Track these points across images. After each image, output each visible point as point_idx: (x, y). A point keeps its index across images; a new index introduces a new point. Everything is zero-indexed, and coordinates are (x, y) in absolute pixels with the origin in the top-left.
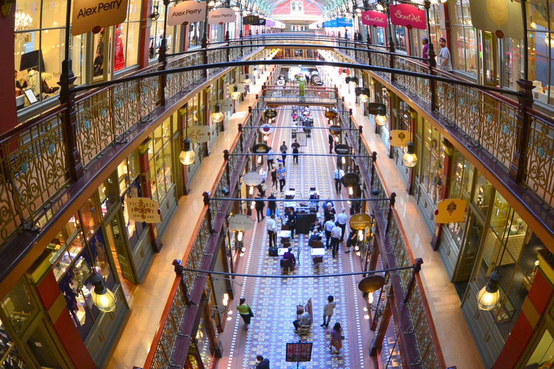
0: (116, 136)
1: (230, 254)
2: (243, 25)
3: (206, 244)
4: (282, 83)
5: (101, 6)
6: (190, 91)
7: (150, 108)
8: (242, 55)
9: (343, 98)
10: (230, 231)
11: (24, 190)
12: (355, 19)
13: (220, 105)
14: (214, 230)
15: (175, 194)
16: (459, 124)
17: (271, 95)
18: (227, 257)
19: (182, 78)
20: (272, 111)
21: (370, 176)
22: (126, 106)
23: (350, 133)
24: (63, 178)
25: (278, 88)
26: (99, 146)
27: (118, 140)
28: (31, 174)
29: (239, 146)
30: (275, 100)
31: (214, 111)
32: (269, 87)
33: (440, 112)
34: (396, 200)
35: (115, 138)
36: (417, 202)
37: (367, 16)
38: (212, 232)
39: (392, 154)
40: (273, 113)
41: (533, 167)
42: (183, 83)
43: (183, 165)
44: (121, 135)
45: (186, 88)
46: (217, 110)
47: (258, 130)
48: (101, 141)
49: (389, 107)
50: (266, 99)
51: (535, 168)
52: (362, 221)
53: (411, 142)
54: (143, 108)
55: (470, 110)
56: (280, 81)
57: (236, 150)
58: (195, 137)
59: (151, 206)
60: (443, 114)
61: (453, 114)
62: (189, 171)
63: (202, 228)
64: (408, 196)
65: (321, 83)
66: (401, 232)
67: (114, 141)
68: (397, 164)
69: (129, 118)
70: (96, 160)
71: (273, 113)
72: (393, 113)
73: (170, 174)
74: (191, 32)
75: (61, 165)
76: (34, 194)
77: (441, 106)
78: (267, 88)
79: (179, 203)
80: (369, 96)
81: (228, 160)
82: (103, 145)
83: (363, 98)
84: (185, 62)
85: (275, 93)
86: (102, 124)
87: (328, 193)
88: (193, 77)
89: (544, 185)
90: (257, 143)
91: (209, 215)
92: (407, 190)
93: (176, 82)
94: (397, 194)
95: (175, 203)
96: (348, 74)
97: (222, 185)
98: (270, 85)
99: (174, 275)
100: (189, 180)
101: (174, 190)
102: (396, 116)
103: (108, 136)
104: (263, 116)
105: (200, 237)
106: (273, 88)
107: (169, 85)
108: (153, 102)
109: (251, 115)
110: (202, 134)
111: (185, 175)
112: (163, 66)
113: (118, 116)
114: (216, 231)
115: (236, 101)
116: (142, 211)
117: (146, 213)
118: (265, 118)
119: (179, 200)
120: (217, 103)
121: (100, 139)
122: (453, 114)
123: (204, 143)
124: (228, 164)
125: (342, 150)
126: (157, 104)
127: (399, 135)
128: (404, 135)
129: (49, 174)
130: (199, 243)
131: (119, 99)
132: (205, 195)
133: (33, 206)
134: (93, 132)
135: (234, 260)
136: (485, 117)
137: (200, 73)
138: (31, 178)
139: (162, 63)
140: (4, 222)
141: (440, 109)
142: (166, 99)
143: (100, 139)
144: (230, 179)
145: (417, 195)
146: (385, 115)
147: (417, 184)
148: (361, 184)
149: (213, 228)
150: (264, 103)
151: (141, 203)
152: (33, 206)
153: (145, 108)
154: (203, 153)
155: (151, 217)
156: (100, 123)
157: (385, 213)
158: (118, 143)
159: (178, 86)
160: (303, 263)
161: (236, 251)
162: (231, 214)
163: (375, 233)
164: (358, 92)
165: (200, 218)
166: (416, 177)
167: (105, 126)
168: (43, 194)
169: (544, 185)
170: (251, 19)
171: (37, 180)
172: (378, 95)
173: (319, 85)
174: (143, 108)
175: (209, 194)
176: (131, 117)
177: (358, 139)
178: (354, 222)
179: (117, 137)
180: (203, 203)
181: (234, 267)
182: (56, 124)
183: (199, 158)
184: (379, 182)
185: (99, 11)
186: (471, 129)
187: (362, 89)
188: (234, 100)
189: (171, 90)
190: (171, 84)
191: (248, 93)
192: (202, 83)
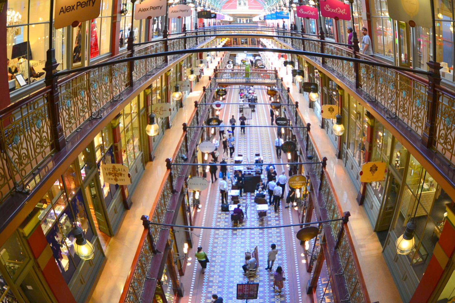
0: (92, 113)
2: (197, 18)
4: (231, 66)
5: (79, 4)
6: (154, 74)
7: (120, 89)
8: (197, 44)
9: (282, 78)
11: (17, 158)
12: (291, 12)
13: (179, 86)
16: (379, 99)
18: (187, 212)
19: (147, 63)
20: (222, 90)
21: (305, 143)
23: (288, 108)
24: (48, 148)
25: (227, 71)
26: (78, 121)
27: (94, 116)
28: (22, 145)
29: (195, 120)
30: (225, 81)
32: (219, 70)
33: (363, 89)
36: (344, 165)
37: (301, 10)
38: (173, 192)
39: (324, 125)
40: (223, 92)
41: (442, 135)
42: (147, 68)
43: (148, 136)
44: (97, 112)
45: (150, 72)
46: (177, 90)
47: (211, 106)
48: (80, 117)
49: (321, 85)
50: (218, 81)
51: (443, 135)
52: (299, 181)
53: (339, 115)
54: (114, 89)
59: (123, 170)
60: (365, 91)
61: (374, 90)
62: (154, 141)
64: (337, 159)
65: (263, 67)
66: (331, 190)
67: (91, 116)
69: (103, 97)
70: (76, 133)
71: (223, 92)
74: (154, 25)
75: (47, 137)
76: (25, 162)
77: (363, 84)
78: (218, 71)
79: (145, 168)
81: (186, 131)
82: (81, 120)
83: (299, 78)
84: (149, 50)
85: (225, 75)
86: (81, 103)
88: (156, 63)
89: (451, 149)
91: (171, 178)
93: (142, 66)
94: (328, 159)
95: (143, 168)
96: (286, 59)
97: (181, 152)
98: (221, 68)
99: (143, 228)
100: (154, 149)
102: (326, 93)
103: (86, 113)
104: (215, 95)
106: (223, 71)
108: (123, 84)
109: (205, 94)
110: (164, 109)
113: (94, 96)
115: (192, 82)
116: (115, 175)
117: (118, 176)
118: (217, 96)
119: (146, 165)
121: (79, 115)
122: (374, 90)
123: (166, 118)
124: (186, 135)
125: (282, 122)
126: (126, 86)
127: (329, 109)
129: (37, 145)
130: (163, 201)
131: (94, 81)
133: (23, 172)
134: (73, 109)
135: (193, 215)
137: (162, 59)
138: (22, 148)
139: (130, 51)
140: (24, 164)
141: (363, 86)
142: (133, 81)
143: (79, 115)
144: (188, 147)
145: (345, 159)
147: (344, 150)
148: (298, 151)
149: (174, 188)
150: (216, 84)
151: (114, 168)
152: (23, 172)
153: (116, 89)
155: (122, 180)
156: (79, 102)
157: (318, 174)
158: (94, 119)
159: (144, 70)
161: (194, 208)
162: (189, 177)
163: (310, 191)
164: (295, 73)
165: (163, 180)
167: (83, 105)
168: (32, 162)
169: (451, 149)
170: (204, 14)
171: (27, 150)
172: (311, 75)
173: (262, 68)
174: (114, 89)
175: (171, 160)
176: (105, 97)
177: (295, 113)
179: (93, 113)
180: (166, 168)
181: (192, 220)
182: (42, 103)
183: (162, 130)
184: (313, 148)
186: (389, 103)
187: (298, 71)
189: (138, 74)
190: (138, 69)
191: (202, 75)
192: (163, 67)
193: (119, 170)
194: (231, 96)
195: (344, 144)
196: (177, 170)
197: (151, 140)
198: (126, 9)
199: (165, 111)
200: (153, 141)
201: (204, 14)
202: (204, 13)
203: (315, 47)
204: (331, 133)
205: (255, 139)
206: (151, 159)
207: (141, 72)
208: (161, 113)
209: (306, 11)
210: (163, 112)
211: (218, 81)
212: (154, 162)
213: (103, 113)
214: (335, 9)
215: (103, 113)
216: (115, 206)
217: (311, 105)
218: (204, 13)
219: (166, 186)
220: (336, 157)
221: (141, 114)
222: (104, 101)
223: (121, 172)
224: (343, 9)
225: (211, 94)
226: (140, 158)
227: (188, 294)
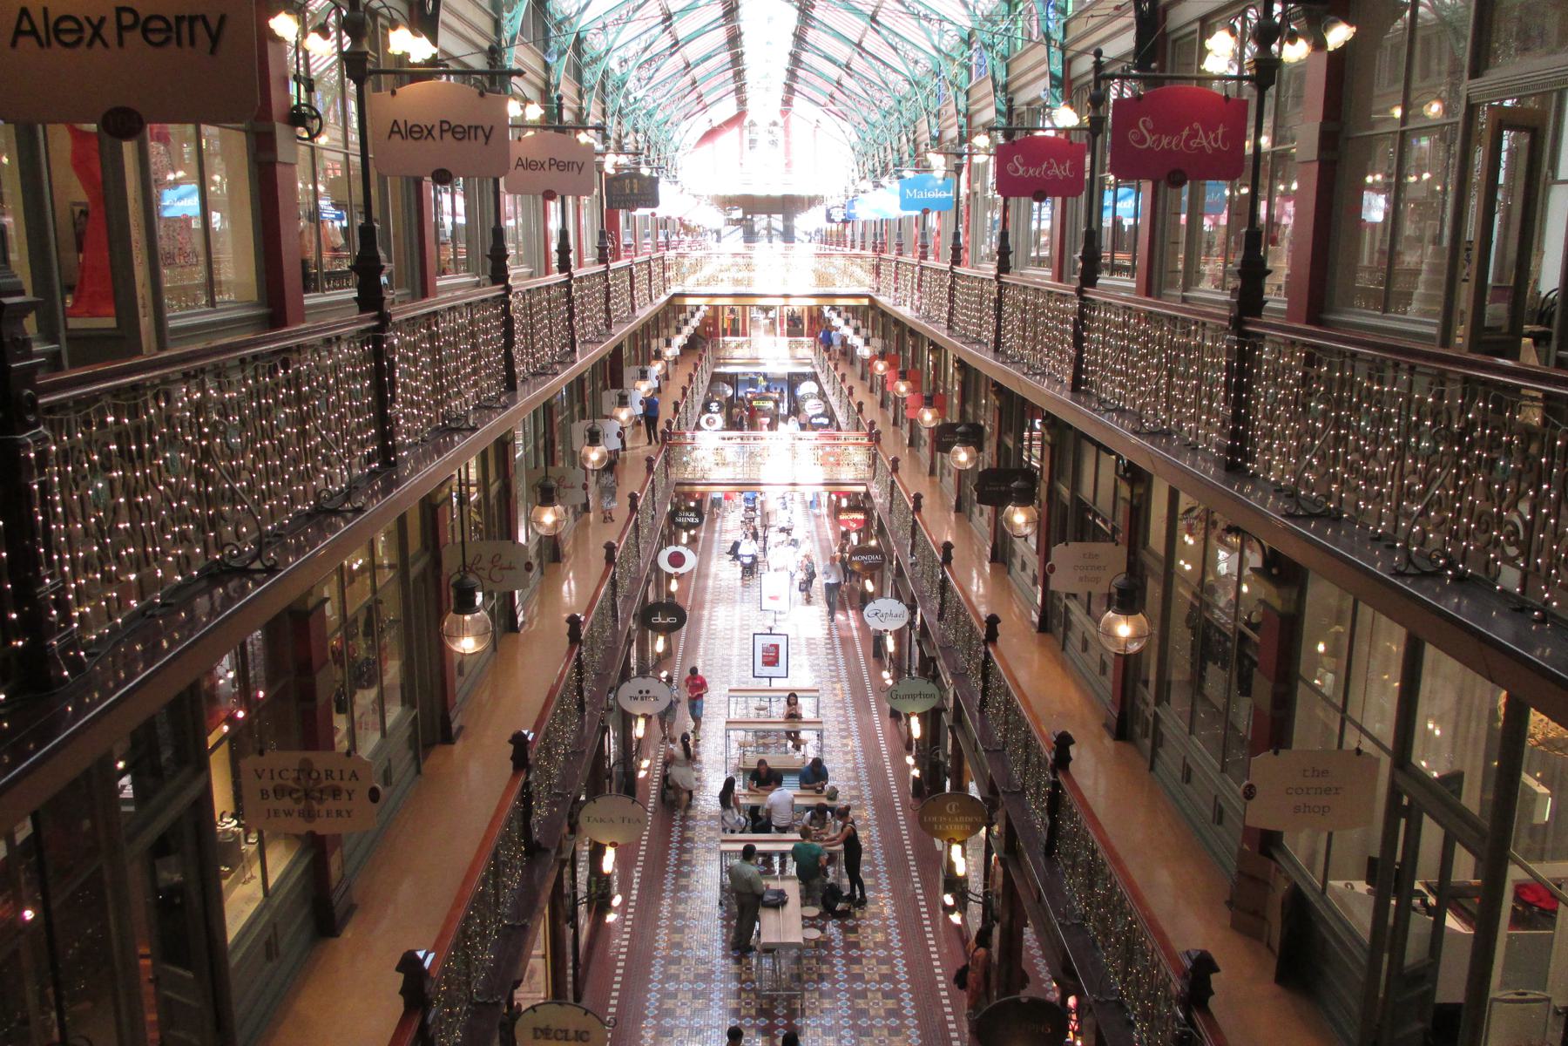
1: (573, 918)
3: (514, 881)
6: (474, 429)
10: (578, 848)
13: (554, 483)
14: (538, 843)
15: (413, 741)
21: (976, 683)
31: (539, 500)
36: (1148, 766)
37: (1017, 160)
39: (1051, 621)
46: (547, 496)
47: (655, 562)
52: (958, 816)
56: (708, 415)
58: (485, 574)
59: (346, 776)
62: (461, 673)
63: (506, 838)
64: (1108, 742)
66: (1102, 854)
72: (1058, 493)
73: (398, 681)
79: (423, 768)
80: (980, 448)
81: (581, 643)
90: (651, 598)
91: (527, 798)
92: (1106, 726)
95: (413, 769)
99: (397, 1006)
100: (458, 699)
101: (410, 729)
102: (1068, 503)
105: (497, 870)
110: (506, 564)
111: (449, 683)
112: (374, 329)
116: (307, 795)
117: (320, 801)
119: (426, 757)
120: (547, 477)
123: (504, 595)
132: (519, 741)
145: (1148, 742)
146: (1033, 503)
147: (1142, 707)
148: (945, 710)
151: (306, 769)
155: (339, 813)
163: (1003, 855)
165: (499, 809)
166: (1140, 685)
170: (632, 189)
172: (1010, 442)
184: (1009, 701)
185: (121, 44)
187: (959, 429)
193: (329, 774)
195: (1140, 685)
198: (309, 105)
200: (456, 672)
202: (631, 183)
204: (1079, 646)
206: (446, 736)
208: (496, 575)
209: (1038, 165)
210: (505, 572)
211: (674, 476)
212: (458, 747)
213: (1475, 911)
214: (1176, 131)
215: (1475, 911)
216: (275, 926)
217: (1002, 553)
218: (631, 183)
220: (1105, 733)
221: (414, 571)
223: (337, 782)
224: (1214, 130)
226: (405, 732)
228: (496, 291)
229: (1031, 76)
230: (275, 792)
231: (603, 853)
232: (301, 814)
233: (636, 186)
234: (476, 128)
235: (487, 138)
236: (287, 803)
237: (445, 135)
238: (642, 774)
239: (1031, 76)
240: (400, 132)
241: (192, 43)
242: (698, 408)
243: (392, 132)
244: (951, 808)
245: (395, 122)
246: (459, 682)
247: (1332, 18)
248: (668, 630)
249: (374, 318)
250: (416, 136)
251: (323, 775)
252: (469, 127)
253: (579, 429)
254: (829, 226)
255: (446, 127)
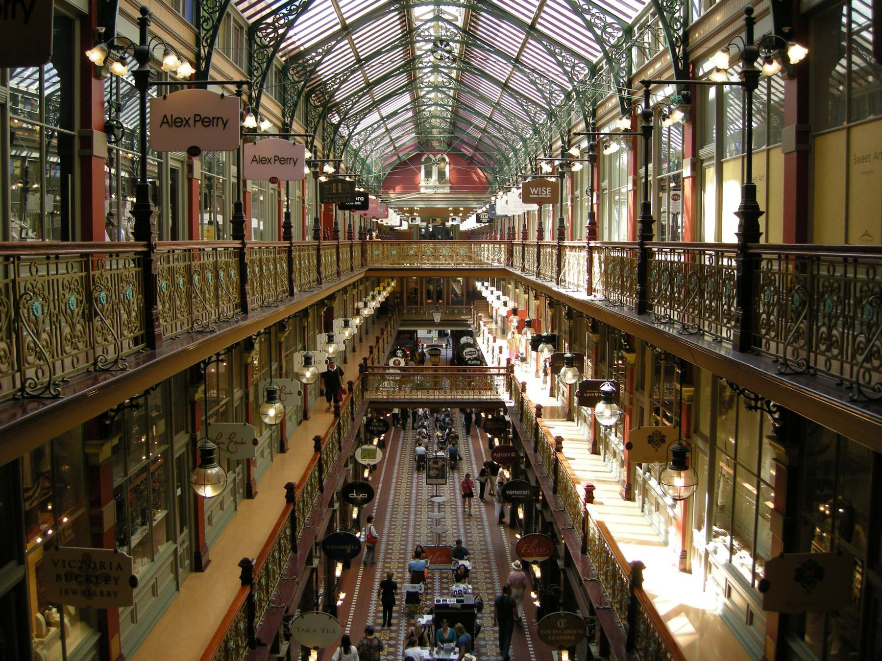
9: (524, 384)
14: (259, 640)
16: (821, 359)
17: (378, 389)
22: (54, 319)
23: (536, 458)
30: (385, 397)
32: (373, 368)
34: (644, 576)
35: (23, 384)
40: (381, 424)
41: (822, 335)
43: (196, 496)
47: (353, 458)
50: (370, 396)
54: (99, 339)
55: (854, 318)
56: (395, 358)
57: (309, 488)
59: (115, 566)
61: (802, 342)
62: (210, 523)
67: (22, 389)
68: (642, 511)
69: (63, 351)
77: (767, 334)
80: (581, 370)
83: (569, 375)
87: (488, 581)
91: (250, 608)
94: (645, 564)
98: (376, 364)
101: (172, 558)
104: (362, 430)
107: (164, 305)
108: (125, 332)
114: (262, 642)
118: (365, 436)
122: (802, 342)
124: (293, 512)
125: (518, 492)
127: (650, 437)
128: (664, 436)
136: (859, 311)
141: (764, 341)
144: (298, 542)
150: (363, 403)
154: (241, 490)
155: (109, 594)
157: (621, 608)
159: (185, 314)
160: (490, 564)
162: (297, 613)
164: (556, 365)
165: (230, 611)
170: (337, 190)
175: (254, 563)
176: (68, 349)
177: (552, 466)
178: (549, 632)
179: (29, 382)
180: (240, 581)
183: (232, 498)
188: (305, 385)
189: (169, 320)
190: (167, 305)
193: (102, 565)
194: (394, 464)
196: (268, 592)
197: (203, 520)
199: (242, 443)
201: (337, 190)
202: (337, 186)
203: (622, 270)
205: (397, 565)
207: (177, 318)
208: (232, 447)
211: (368, 397)
219: (236, 627)
222: (68, 362)
225: (353, 427)
227: (638, 318)
228: (237, 244)
229: (609, 116)
230: (66, 575)
231: (309, 654)
232: (83, 593)
233: (340, 187)
234: (218, 118)
235: (225, 125)
236: (73, 585)
237: (197, 124)
238: (339, 603)
239: (609, 116)
240: (168, 122)
241: (14, 16)
242: (387, 353)
243: (163, 122)
244: (561, 624)
245: (165, 116)
246: (207, 528)
247: (791, 43)
248: (359, 504)
249: (144, 246)
250: (179, 124)
251: (98, 566)
252: (214, 118)
253: (298, 358)
254: (479, 225)
255: (198, 118)
